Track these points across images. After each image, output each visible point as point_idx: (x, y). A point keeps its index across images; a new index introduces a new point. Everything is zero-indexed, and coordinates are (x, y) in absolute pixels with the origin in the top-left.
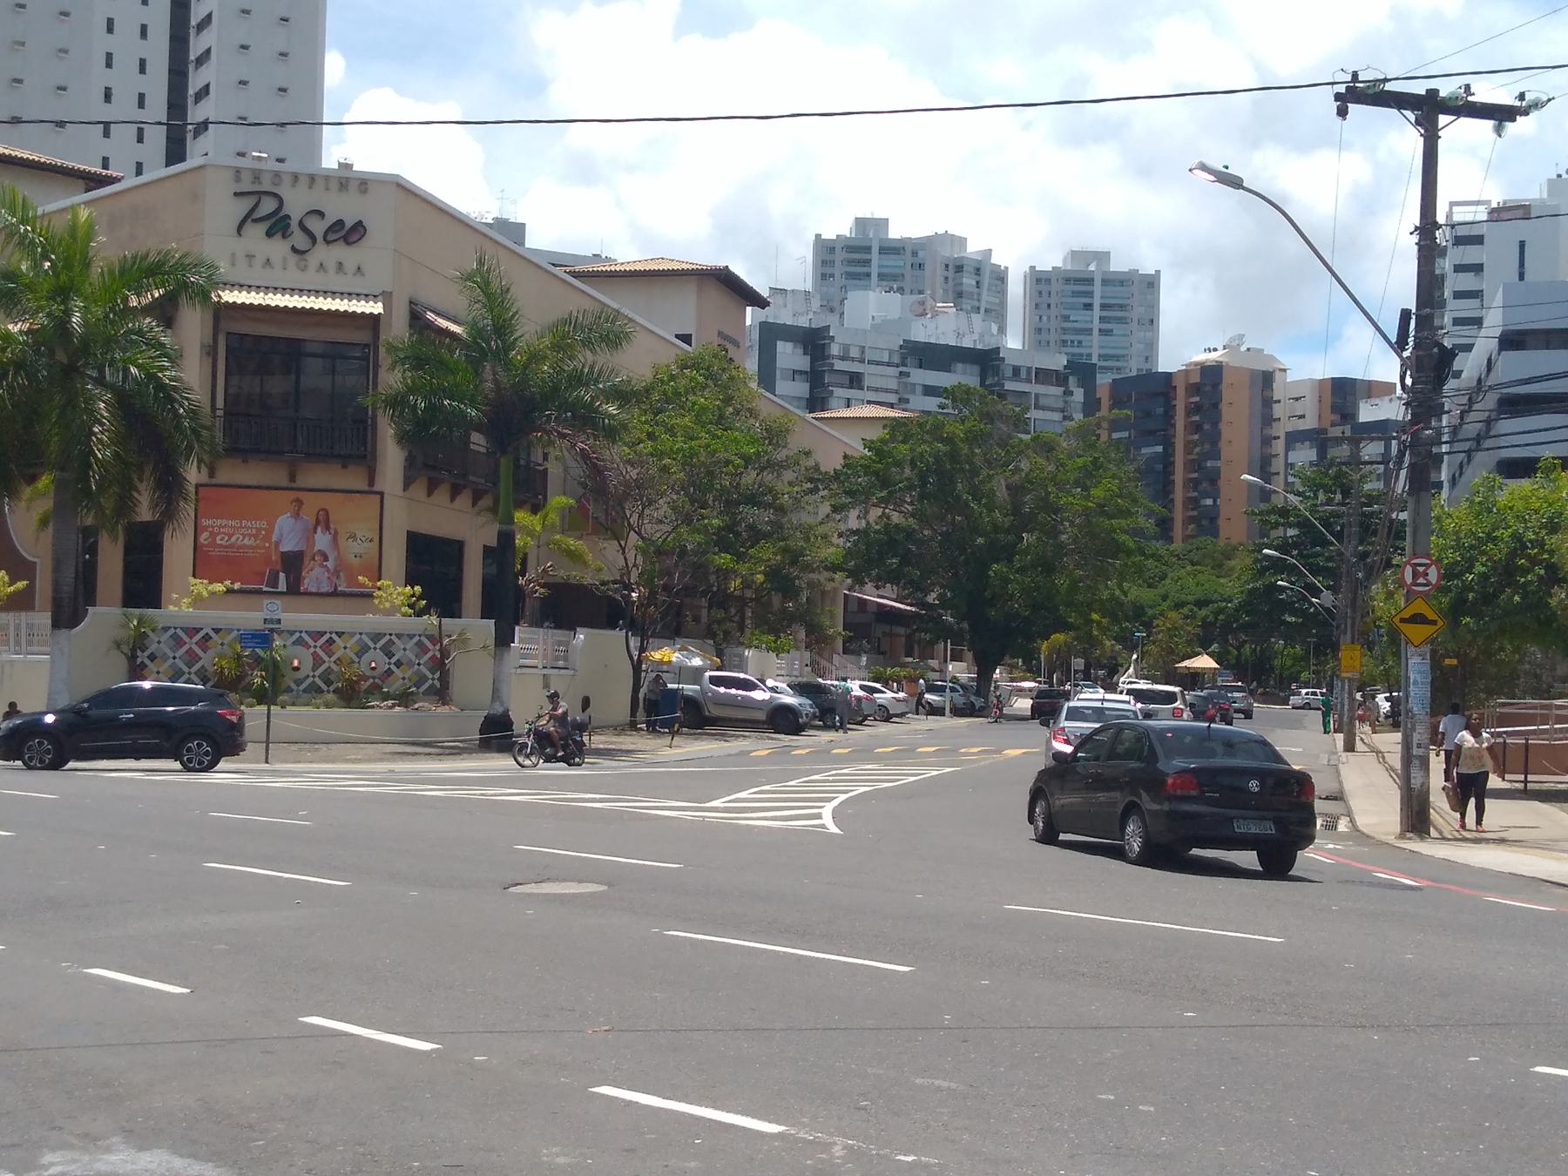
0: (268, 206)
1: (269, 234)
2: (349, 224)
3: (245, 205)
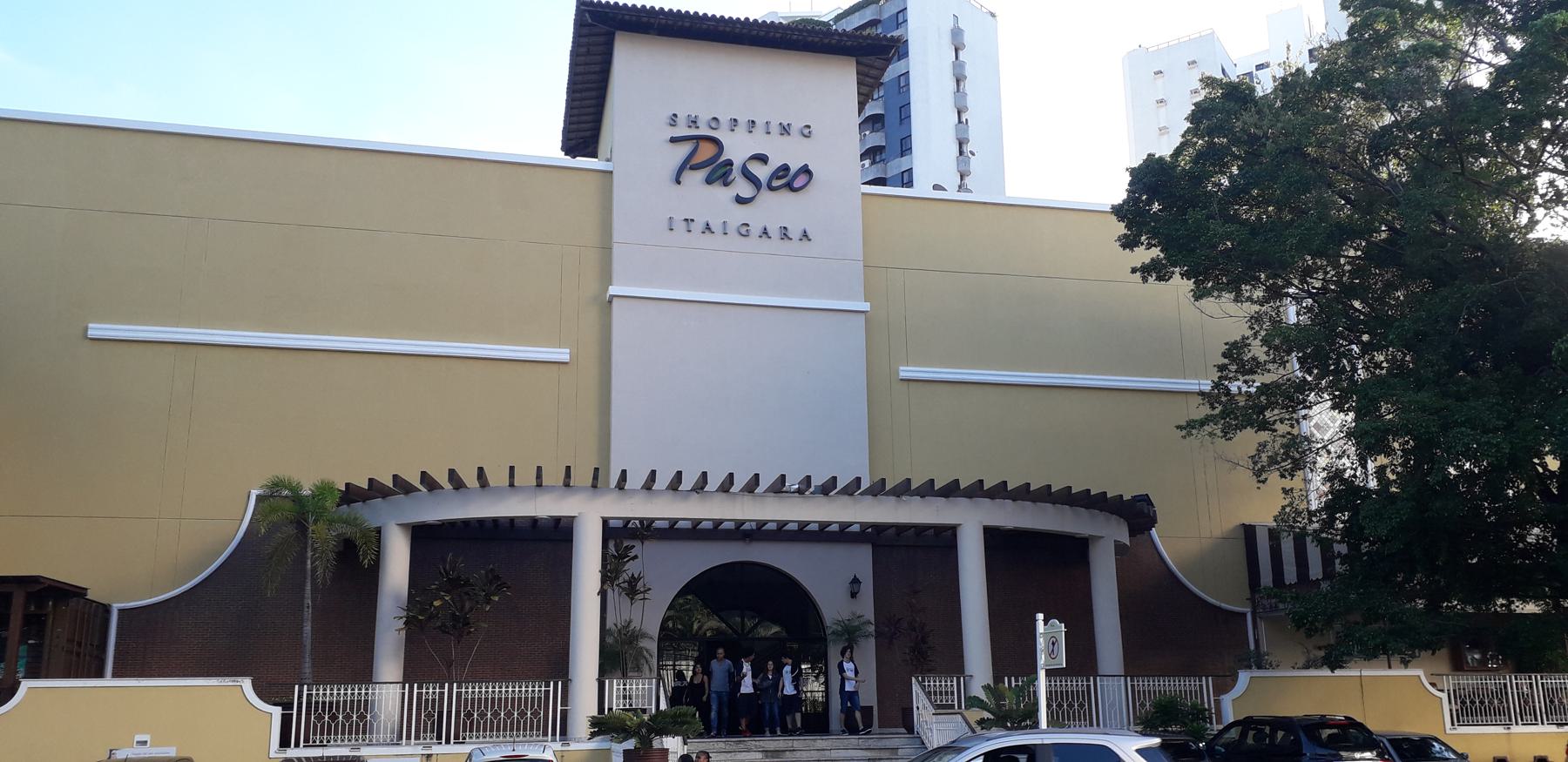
0: (707, 151)
1: (709, 181)
2: (794, 168)
3: (684, 150)
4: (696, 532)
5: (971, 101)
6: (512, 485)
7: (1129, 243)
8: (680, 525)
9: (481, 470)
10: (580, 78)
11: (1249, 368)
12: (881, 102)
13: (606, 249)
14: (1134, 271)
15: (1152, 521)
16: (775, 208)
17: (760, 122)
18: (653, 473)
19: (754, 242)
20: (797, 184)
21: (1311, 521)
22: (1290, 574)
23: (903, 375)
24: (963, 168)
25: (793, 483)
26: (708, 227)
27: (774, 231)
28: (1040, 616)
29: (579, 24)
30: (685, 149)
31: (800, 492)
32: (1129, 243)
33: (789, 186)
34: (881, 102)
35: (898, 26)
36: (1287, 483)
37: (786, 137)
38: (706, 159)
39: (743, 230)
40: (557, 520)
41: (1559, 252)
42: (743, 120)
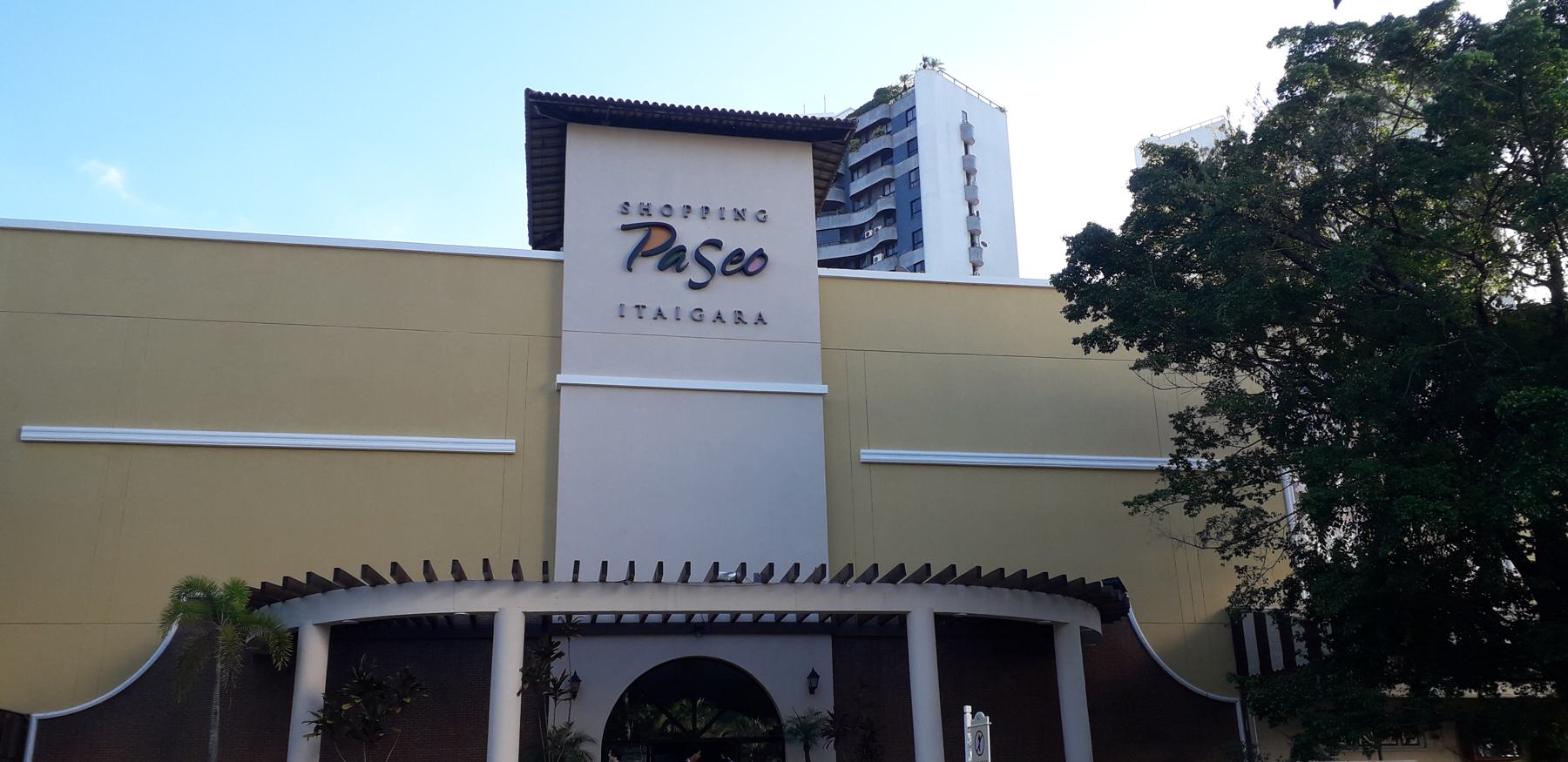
0: (659, 238)
1: (662, 267)
2: (748, 252)
4: (643, 627)
5: (982, 194)
6: (575, 580)
7: (1074, 314)
8: (742, 618)
9: (427, 563)
10: (538, 171)
11: (1208, 441)
12: (892, 198)
13: (556, 337)
14: (1076, 341)
15: (1124, 608)
16: (730, 293)
17: (714, 209)
18: (688, 565)
19: (707, 328)
20: (751, 269)
21: (1268, 601)
22: (1277, 662)
23: (864, 458)
24: (975, 259)
25: (728, 571)
26: (660, 313)
27: (728, 316)
28: (968, 709)
29: (530, 117)
30: (637, 236)
31: (738, 580)
32: (1074, 314)
33: (744, 271)
34: (892, 198)
35: (907, 123)
36: (1241, 561)
37: (740, 223)
38: (658, 245)
39: (697, 315)
40: (473, 617)
41: (1567, 325)
42: (696, 207)
